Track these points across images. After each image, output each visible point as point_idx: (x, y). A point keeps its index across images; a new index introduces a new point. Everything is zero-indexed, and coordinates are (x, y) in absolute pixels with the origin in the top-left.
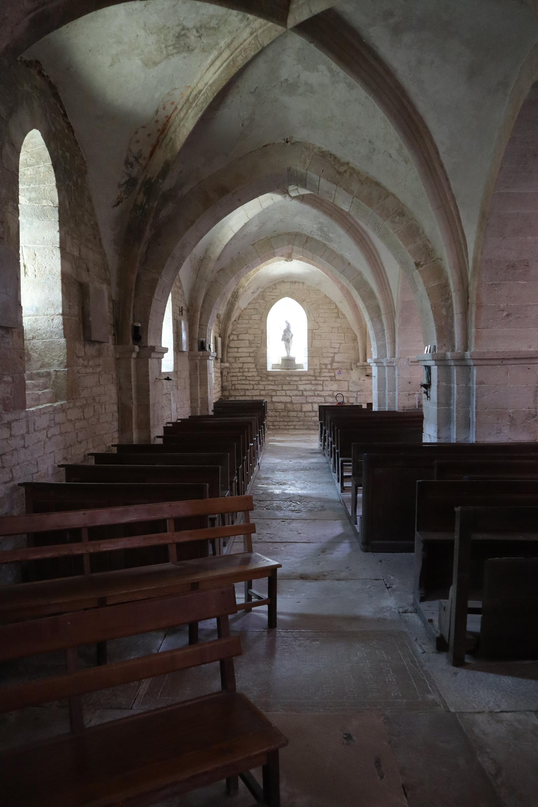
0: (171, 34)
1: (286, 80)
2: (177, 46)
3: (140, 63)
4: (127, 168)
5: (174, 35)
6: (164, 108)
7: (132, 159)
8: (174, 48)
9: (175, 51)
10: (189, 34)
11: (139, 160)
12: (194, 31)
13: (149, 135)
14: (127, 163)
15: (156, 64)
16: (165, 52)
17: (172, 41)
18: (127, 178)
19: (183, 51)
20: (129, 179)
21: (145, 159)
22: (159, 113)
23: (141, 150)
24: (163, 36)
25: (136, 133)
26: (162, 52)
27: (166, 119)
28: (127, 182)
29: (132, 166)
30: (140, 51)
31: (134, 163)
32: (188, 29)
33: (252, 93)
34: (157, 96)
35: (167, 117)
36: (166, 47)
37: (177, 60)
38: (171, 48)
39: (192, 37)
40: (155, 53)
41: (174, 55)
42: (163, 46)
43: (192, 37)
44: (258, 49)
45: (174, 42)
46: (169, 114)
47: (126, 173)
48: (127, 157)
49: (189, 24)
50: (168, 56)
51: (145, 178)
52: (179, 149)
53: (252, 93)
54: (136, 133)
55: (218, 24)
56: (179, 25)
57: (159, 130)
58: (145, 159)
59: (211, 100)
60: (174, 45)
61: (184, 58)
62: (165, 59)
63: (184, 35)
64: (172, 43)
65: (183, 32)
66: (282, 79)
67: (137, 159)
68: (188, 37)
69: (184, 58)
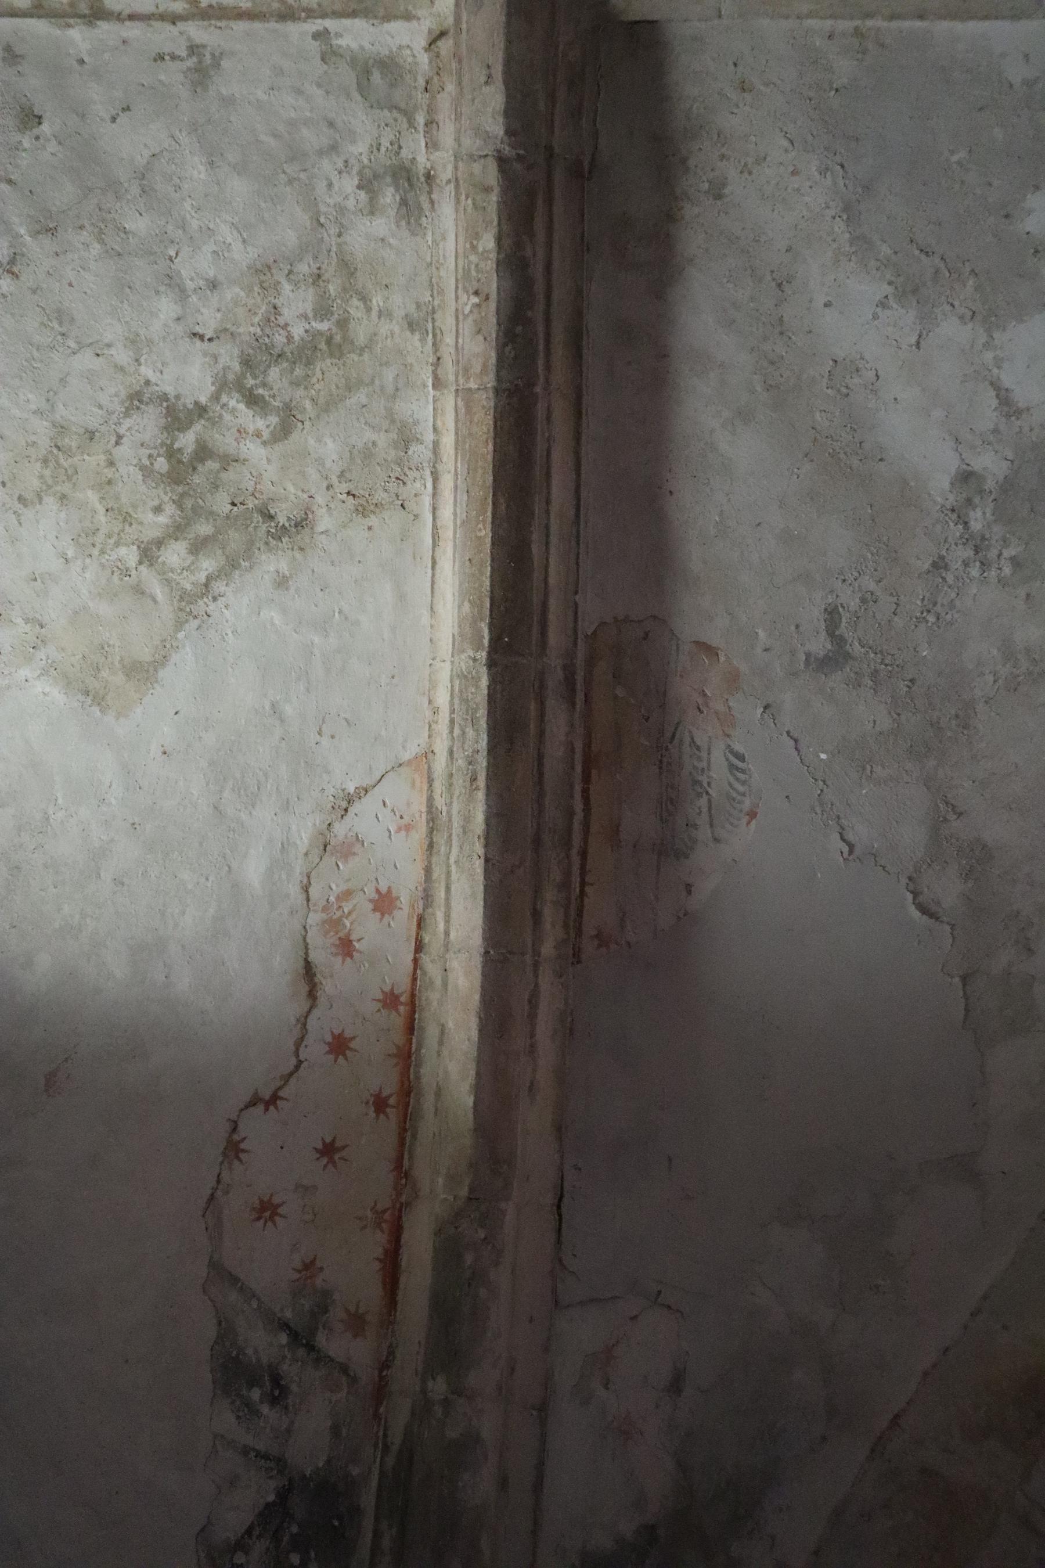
0: (129, 472)
1: (966, 477)
2: (204, 529)
3: (57, 695)
4: (248, 1412)
5: (147, 471)
6: (346, 947)
7: (261, 1344)
8: (198, 547)
9: (208, 565)
10: (224, 441)
11: (321, 1339)
12: (234, 402)
13: (328, 1150)
14: (234, 1373)
15: (144, 672)
16: (158, 591)
17: (158, 510)
18: (256, 1491)
19: (248, 550)
20: (283, 1495)
21: (357, 1323)
22: (328, 987)
23: (309, 1266)
24: (92, 496)
25: (233, 1150)
26: (139, 591)
27: (397, 1020)
28: (272, 1517)
29: (278, 1392)
30: (23, 627)
31: (289, 1369)
32: (201, 410)
33: (826, 664)
34: (253, 871)
35: (390, 1000)
36: (148, 554)
37: (245, 607)
38: (175, 554)
39: (253, 451)
40: (104, 609)
41: (219, 587)
42: (130, 555)
43: (253, 451)
44: (487, 190)
45: (170, 509)
46: (403, 985)
47: (246, 1451)
48: (226, 1331)
49: (192, 377)
50: (191, 602)
51: (386, 1448)
52: (470, 1101)
53: (826, 664)
54: (233, 1150)
55: (323, 311)
56: (136, 400)
57: (380, 1104)
58: (357, 1323)
59: (484, 682)
60: (177, 531)
61: (282, 582)
62: (179, 625)
63: (203, 452)
64: (162, 519)
65: (187, 441)
66: (940, 485)
67: (302, 1339)
68: (228, 461)
69: (282, 582)
